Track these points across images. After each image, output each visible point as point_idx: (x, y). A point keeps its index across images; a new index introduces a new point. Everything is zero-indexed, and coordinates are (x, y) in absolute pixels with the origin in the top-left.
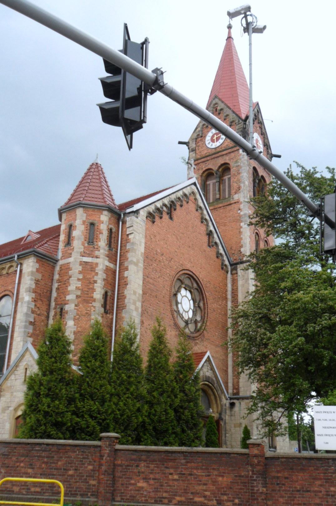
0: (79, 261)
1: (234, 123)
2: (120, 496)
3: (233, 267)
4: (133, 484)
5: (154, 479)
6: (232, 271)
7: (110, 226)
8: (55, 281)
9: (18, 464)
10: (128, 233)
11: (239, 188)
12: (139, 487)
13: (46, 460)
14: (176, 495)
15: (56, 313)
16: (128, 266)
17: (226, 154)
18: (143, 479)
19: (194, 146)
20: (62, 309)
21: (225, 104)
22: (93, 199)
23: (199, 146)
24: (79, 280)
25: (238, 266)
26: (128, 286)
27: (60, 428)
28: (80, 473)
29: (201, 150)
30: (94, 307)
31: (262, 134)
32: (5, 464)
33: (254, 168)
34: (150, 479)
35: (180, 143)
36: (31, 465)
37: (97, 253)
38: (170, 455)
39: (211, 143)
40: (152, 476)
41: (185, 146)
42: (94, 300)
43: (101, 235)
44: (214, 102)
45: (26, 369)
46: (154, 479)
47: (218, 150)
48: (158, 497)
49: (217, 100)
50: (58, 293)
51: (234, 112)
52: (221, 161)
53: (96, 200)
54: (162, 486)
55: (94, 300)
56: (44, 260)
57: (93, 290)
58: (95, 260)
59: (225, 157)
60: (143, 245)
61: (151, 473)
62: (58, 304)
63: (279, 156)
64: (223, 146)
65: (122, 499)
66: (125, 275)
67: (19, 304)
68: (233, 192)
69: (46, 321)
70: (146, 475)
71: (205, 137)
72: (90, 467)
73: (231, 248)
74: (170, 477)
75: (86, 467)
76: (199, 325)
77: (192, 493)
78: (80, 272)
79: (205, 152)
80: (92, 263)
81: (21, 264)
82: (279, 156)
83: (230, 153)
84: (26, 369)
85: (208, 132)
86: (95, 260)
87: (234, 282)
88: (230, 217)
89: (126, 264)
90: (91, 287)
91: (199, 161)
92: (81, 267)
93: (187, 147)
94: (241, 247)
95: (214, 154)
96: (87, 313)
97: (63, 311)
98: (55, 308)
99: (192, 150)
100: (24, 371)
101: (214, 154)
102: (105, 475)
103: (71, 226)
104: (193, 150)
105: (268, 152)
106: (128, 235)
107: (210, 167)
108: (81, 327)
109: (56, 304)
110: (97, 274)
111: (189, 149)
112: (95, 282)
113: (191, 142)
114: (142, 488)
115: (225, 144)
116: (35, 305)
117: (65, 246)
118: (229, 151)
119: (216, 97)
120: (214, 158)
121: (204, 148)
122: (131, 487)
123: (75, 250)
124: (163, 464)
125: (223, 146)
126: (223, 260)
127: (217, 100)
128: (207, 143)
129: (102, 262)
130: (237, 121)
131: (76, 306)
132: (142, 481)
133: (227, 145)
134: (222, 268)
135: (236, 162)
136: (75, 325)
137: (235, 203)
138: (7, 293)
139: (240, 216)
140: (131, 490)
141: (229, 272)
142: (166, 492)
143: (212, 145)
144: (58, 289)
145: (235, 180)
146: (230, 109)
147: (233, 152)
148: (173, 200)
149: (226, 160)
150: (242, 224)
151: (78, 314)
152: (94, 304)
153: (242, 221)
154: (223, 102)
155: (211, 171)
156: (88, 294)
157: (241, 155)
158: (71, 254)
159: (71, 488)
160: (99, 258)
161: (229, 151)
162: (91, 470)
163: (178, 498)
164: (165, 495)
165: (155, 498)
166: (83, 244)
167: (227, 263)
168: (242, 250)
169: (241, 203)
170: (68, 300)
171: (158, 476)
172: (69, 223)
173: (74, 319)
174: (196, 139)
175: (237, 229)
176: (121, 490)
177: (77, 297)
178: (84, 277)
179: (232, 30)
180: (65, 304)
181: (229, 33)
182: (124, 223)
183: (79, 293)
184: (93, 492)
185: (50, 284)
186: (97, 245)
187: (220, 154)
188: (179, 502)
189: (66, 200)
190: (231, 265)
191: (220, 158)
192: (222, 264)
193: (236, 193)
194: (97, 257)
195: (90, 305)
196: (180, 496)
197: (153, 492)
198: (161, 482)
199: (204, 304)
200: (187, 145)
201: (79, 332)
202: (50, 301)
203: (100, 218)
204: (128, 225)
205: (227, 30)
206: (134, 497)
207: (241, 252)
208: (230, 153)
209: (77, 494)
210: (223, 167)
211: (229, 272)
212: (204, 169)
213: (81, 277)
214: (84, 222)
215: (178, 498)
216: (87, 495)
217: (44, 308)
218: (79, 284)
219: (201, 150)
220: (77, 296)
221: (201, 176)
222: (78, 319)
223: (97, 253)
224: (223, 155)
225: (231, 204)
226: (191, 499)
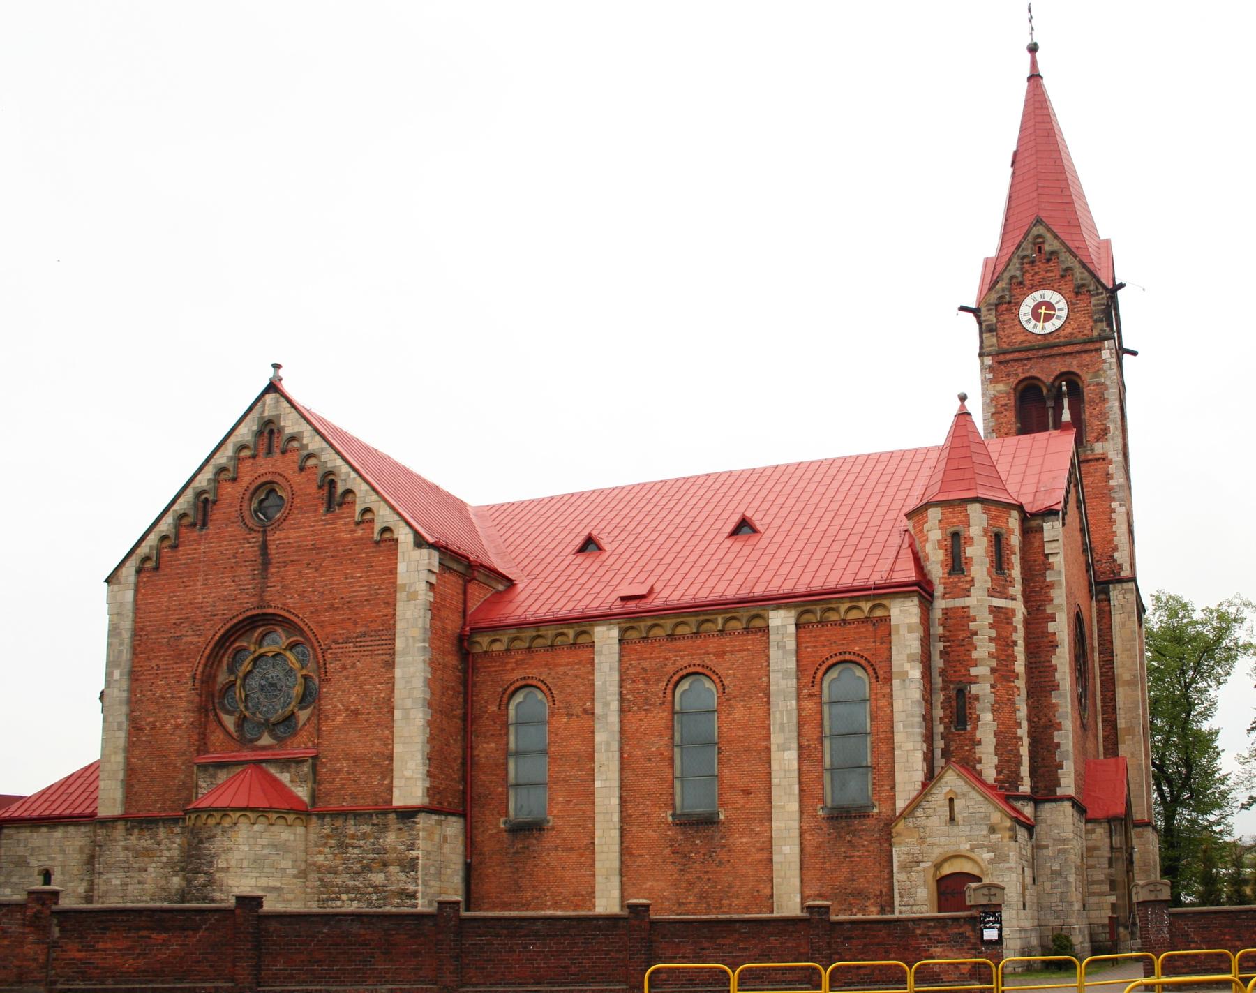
0: (987, 605)
1: (1083, 290)
3: (1100, 587)
11: (1106, 431)
17: (1071, 354)
19: (992, 319)
21: (1063, 243)
23: (1003, 322)
24: (991, 639)
29: (1008, 331)
37: (1011, 590)
39: (1033, 322)
41: (971, 315)
42: (1017, 677)
44: (1035, 231)
45: (951, 800)
47: (1052, 340)
49: (1040, 230)
51: (1084, 266)
52: (1058, 366)
55: (1017, 677)
59: (1068, 360)
62: (951, 682)
63: (963, 309)
64: (1062, 333)
71: (1018, 304)
78: (992, 626)
79: (1021, 338)
82: (963, 309)
83: (1079, 352)
84: (951, 800)
85: (1026, 295)
91: (1008, 357)
93: (974, 319)
94: (1115, 549)
95: (1045, 348)
100: (947, 802)
101: (1045, 348)
104: (991, 329)
107: (1034, 373)
108: (1003, 724)
110: (1015, 629)
111: (980, 323)
112: (1015, 643)
113: (984, 310)
117: (949, 574)
118: (1078, 347)
119: (1039, 221)
120: (1043, 357)
121: (1017, 329)
123: (977, 584)
125: (1062, 333)
127: (1040, 230)
128: (1023, 319)
130: (1092, 288)
131: (992, 687)
133: (1071, 334)
135: (1096, 374)
137: (1097, 460)
139: (1111, 489)
144: (944, 654)
145: (1095, 412)
146: (1076, 257)
147: (1086, 352)
149: (1071, 365)
150: (1114, 505)
151: (996, 702)
153: (1113, 500)
154: (1056, 237)
155: (1036, 382)
157: (1104, 361)
158: (969, 590)
161: (1078, 347)
166: (989, 573)
168: (1116, 555)
169: (1111, 462)
170: (977, 676)
172: (953, 529)
173: (993, 711)
174: (996, 305)
175: (1104, 513)
177: (993, 670)
179: (1038, 54)
180: (971, 683)
181: (1034, 64)
191: (1058, 359)
194: (1013, 598)
203: (1007, 522)
205: (1028, 56)
207: (1115, 561)
208: (1079, 352)
212: (1022, 376)
214: (986, 531)
218: (992, 648)
219: (1008, 331)
220: (992, 669)
221: (1015, 389)
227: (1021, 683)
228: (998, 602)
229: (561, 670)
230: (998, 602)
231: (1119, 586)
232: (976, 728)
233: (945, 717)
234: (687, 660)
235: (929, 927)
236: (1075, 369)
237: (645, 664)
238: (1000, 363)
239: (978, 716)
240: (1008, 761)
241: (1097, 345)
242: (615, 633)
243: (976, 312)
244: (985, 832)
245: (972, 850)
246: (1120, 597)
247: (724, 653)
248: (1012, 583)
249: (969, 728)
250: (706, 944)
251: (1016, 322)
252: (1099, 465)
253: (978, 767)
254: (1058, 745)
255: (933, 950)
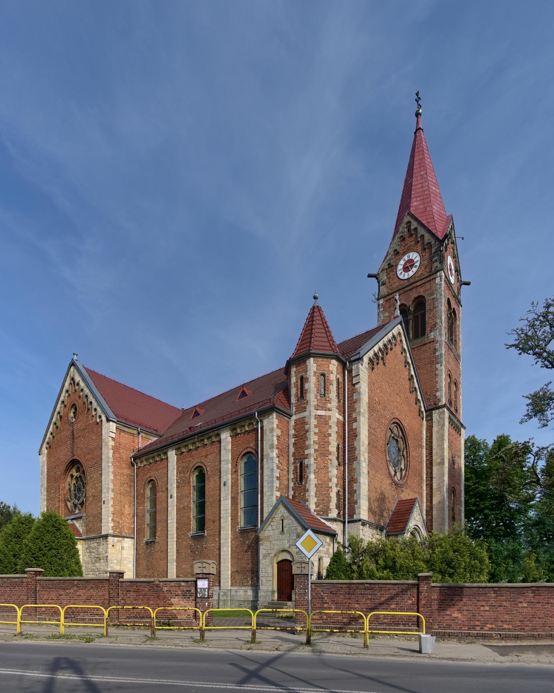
2: (437, 625)
4: (449, 615)
5: (466, 610)
6: (427, 416)
7: (338, 376)
8: (291, 436)
9: (346, 600)
10: (354, 383)
11: (435, 325)
12: (454, 617)
13: (370, 596)
14: (488, 624)
15: (296, 468)
16: (356, 418)
18: (458, 610)
20: (301, 464)
22: (321, 348)
25: (433, 412)
26: (357, 438)
27: (120, 573)
28: (401, 607)
30: (331, 460)
31: (454, 257)
32: (334, 601)
33: (448, 299)
34: (463, 610)
35: (370, 276)
36: (357, 601)
37: (329, 405)
38: (481, 590)
40: (465, 608)
42: (330, 453)
43: (331, 386)
46: (466, 610)
47: (412, 281)
48: (471, 625)
50: (296, 449)
53: (324, 348)
54: (474, 616)
55: (330, 453)
56: (281, 416)
57: (329, 443)
58: (328, 413)
60: (367, 394)
61: (465, 606)
62: (297, 459)
64: (417, 275)
65: (439, 627)
66: (354, 427)
67: (265, 460)
68: (428, 329)
69: (287, 476)
70: (460, 608)
72: (410, 602)
73: (426, 393)
74: (482, 608)
75: (407, 602)
76: (404, 473)
77: (501, 621)
80: (325, 416)
81: (261, 421)
84: (282, 520)
85: (400, 259)
86: (328, 413)
87: (430, 429)
88: (424, 358)
89: (354, 415)
90: (326, 440)
92: (316, 421)
94: (437, 391)
96: (324, 466)
97: (303, 465)
98: (294, 463)
99: (381, 284)
102: (424, 607)
103: (302, 378)
105: (458, 279)
106: (354, 385)
108: (320, 480)
109: (294, 459)
110: (330, 427)
111: (379, 282)
112: (330, 435)
114: (457, 618)
115: (419, 273)
116: (279, 461)
117: (298, 400)
122: (447, 618)
124: (475, 598)
126: (420, 406)
128: (399, 273)
129: (336, 416)
132: (456, 612)
134: (419, 415)
136: (315, 478)
137: (430, 342)
138: (200, 464)
140: (447, 620)
141: (425, 419)
142: (478, 621)
143: (404, 275)
144: (295, 444)
148: (386, 343)
149: (420, 292)
152: (330, 457)
156: (324, 448)
158: (305, 408)
159: (394, 619)
160: (331, 410)
161: (424, 281)
162: (411, 604)
163: (489, 626)
164: (477, 623)
165: (468, 626)
167: (423, 409)
171: (470, 608)
176: (438, 620)
178: (320, 430)
180: (305, 459)
182: (350, 372)
183: (316, 447)
184: (413, 622)
185: (287, 440)
186: (328, 397)
187: (414, 285)
188: (490, 629)
189: (293, 351)
190: (426, 411)
192: (420, 410)
193: (431, 331)
194: (329, 410)
195: (327, 458)
196: (491, 624)
197: (467, 621)
198: (473, 613)
199: (407, 452)
200: (377, 279)
201: (319, 484)
202: (288, 456)
204: (354, 374)
206: (450, 625)
209: (400, 624)
210: (416, 301)
211: (425, 419)
213: (317, 430)
215: (489, 626)
216: (409, 624)
217: (285, 463)
222: (318, 471)
223: (329, 405)
224: (417, 287)
225: (425, 344)
226: (501, 626)
227: (333, 457)
228: (320, 413)
229: (160, 471)
230: (320, 413)
231: (437, 411)
232: (306, 483)
233: (294, 478)
234: (196, 461)
235: (172, 586)
236: (422, 294)
237: (184, 465)
238: (386, 301)
239: (308, 476)
240: (323, 500)
241: (434, 276)
242: (174, 452)
243: (516, 346)
244: (295, 538)
245: (289, 547)
246: (438, 417)
247: (207, 455)
248: (329, 401)
249: (303, 483)
250: (62, 593)
251: (396, 276)
252: (431, 345)
253: (307, 503)
254: (355, 491)
255: (172, 600)
